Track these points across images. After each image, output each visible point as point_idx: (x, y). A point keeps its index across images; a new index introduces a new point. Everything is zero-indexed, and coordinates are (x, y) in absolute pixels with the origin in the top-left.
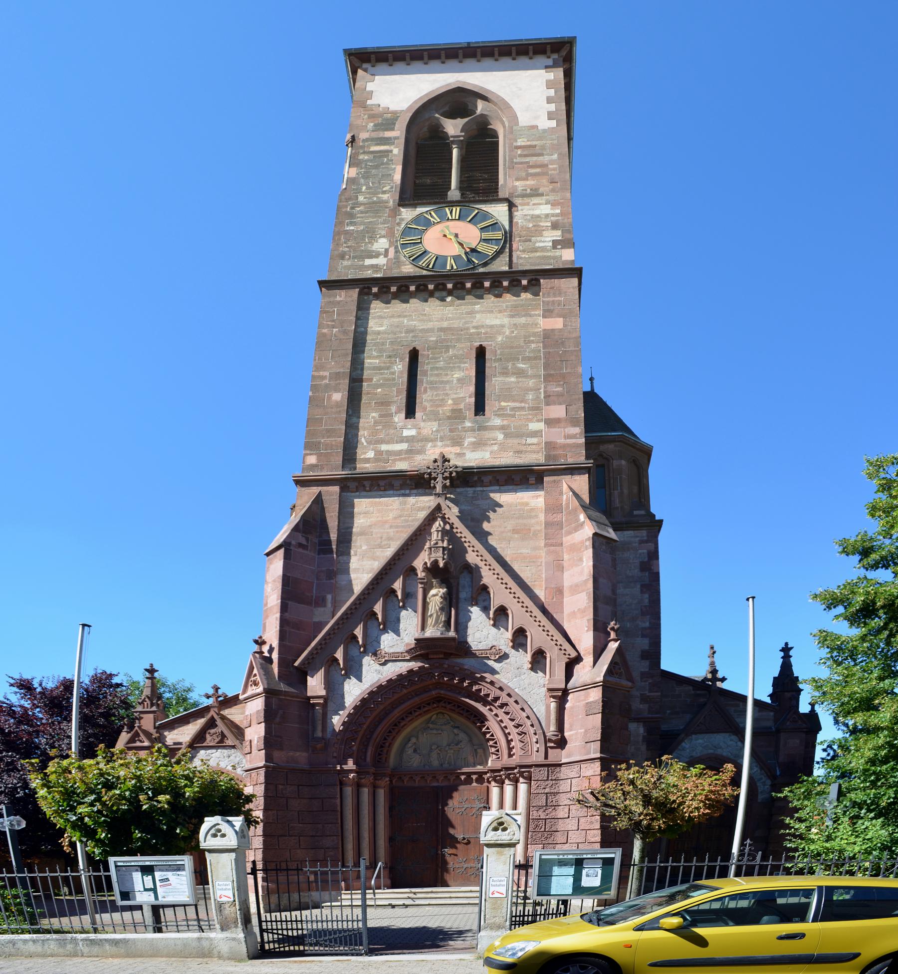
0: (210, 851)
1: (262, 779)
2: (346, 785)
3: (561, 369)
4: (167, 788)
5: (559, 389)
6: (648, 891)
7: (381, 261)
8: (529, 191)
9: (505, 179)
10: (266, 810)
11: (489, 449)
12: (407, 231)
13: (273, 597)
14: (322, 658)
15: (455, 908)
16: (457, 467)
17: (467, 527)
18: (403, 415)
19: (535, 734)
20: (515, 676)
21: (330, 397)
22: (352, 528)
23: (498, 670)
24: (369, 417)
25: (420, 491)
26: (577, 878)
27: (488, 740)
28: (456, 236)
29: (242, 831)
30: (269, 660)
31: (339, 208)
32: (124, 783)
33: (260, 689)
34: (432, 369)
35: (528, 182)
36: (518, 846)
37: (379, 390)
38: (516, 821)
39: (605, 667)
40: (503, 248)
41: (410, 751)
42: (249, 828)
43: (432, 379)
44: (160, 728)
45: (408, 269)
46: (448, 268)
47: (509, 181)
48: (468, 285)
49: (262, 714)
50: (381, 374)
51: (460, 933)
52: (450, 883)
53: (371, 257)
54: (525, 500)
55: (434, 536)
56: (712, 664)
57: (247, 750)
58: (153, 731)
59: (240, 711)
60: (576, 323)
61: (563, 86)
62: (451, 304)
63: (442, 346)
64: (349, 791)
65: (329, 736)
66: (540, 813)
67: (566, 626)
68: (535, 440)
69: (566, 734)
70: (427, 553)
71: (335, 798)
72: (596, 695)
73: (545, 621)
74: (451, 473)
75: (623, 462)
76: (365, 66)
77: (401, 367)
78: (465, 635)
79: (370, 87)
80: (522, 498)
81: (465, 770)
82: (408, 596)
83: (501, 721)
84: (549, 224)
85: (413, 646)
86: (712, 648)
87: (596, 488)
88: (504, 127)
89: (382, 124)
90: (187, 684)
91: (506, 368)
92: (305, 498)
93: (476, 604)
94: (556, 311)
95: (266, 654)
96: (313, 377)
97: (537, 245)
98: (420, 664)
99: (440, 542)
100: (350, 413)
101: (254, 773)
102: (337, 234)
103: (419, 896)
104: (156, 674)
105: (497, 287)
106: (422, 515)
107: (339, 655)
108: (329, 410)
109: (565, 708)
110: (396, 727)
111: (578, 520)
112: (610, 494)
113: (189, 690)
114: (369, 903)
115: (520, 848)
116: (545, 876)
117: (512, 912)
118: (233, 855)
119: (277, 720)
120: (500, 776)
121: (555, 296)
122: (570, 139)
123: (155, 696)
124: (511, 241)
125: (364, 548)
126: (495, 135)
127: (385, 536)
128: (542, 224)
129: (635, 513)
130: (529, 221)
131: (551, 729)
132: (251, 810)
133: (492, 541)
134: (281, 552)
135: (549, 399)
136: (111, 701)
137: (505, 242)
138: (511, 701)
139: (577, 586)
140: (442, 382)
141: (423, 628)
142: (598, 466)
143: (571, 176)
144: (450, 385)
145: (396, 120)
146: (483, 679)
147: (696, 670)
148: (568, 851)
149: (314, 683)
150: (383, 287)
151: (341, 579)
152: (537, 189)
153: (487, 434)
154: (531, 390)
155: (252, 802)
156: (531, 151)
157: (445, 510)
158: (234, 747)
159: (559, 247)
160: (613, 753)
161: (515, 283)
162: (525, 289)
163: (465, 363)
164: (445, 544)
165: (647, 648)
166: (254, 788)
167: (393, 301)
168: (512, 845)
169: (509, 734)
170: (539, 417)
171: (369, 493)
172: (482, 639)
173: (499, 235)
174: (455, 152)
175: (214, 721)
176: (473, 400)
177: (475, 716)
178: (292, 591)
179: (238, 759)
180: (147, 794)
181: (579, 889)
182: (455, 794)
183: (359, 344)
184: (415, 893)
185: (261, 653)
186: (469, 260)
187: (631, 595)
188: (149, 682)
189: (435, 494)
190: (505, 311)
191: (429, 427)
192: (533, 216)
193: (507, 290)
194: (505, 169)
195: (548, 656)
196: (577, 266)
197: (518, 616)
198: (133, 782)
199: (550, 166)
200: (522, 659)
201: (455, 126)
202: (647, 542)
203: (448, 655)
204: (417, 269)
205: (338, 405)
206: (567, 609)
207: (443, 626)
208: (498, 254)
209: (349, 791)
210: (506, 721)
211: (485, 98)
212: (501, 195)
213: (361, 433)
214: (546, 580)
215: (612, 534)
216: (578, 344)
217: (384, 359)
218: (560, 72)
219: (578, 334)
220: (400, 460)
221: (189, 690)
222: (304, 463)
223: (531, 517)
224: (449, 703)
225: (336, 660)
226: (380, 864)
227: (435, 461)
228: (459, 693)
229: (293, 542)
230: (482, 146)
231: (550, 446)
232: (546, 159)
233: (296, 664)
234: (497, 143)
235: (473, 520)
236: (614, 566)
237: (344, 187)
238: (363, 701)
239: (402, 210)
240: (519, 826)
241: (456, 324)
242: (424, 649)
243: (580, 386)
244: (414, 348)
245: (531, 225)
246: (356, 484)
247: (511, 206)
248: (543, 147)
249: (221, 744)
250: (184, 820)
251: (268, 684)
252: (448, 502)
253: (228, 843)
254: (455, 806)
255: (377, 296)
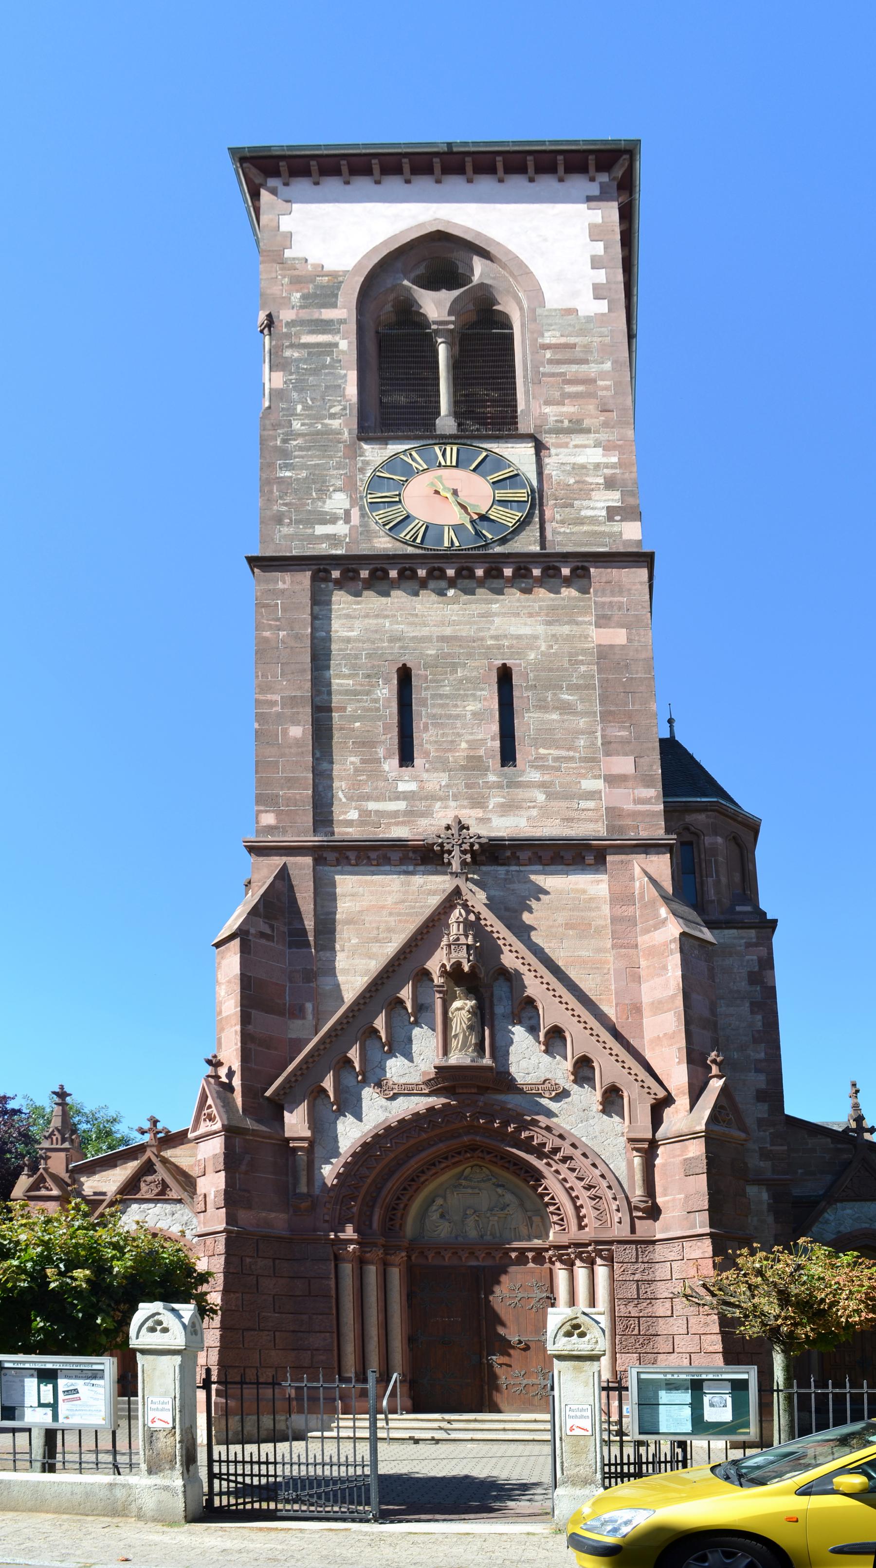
0: (144, 1352)
1: (221, 1247)
2: (344, 1260)
3: (626, 704)
4: (87, 1260)
5: (624, 733)
6: (804, 1431)
7: (340, 529)
8: (566, 423)
9: (527, 402)
10: (226, 1292)
11: (525, 813)
12: (376, 482)
13: (229, 1003)
14: (304, 1087)
15: (513, 1446)
16: (479, 837)
17: (499, 917)
18: (396, 761)
19: (615, 1199)
20: (578, 1117)
21: (285, 732)
22: (335, 913)
23: (556, 1112)
24: (345, 764)
25: (429, 867)
26: (697, 1407)
27: (547, 1205)
28: (455, 493)
29: (193, 1324)
30: (229, 1088)
31: (263, 441)
32: (25, 1250)
33: (218, 1126)
34: (434, 696)
35: (565, 409)
36: (602, 1358)
37: (357, 724)
38: (598, 1323)
39: (707, 1113)
40: (530, 515)
41: (435, 1216)
42: (203, 1319)
43: (434, 711)
44: (76, 1172)
45: (383, 544)
46: (446, 544)
47: (534, 405)
48: (480, 572)
49: (222, 1159)
50: (359, 701)
51: (524, 1488)
52: (502, 1406)
53: (324, 522)
54: (581, 886)
55: (454, 929)
56: (856, 1107)
57: (201, 1207)
58: (65, 1176)
59: (188, 1153)
60: (647, 637)
61: (618, 237)
62: (455, 601)
63: (446, 663)
64: (347, 1269)
65: (317, 1191)
66: (630, 1307)
67: (648, 1056)
68: (591, 804)
69: (660, 1200)
70: (445, 951)
71: (328, 1278)
72: (697, 1149)
73: (617, 1048)
74: (472, 845)
75: (719, 840)
76: (272, 182)
77: (386, 692)
78: (507, 1064)
79: (286, 224)
80: (576, 884)
81: (516, 1245)
82: (422, 1009)
83: (565, 1180)
84: (601, 480)
85: (432, 1076)
86: (854, 1085)
87: (680, 873)
88: (521, 309)
89: (315, 296)
90: (112, 1113)
91: (545, 700)
92: (264, 872)
93: (520, 1023)
94: (615, 618)
95: (224, 1079)
96: (257, 701)
97: (584, 513)
98: (444, 1100)
99: (462, 938)
100: (318, 755)
101: (210, 1240)
102: (266, 483)
103: (456, 1425)
104: (68, 1099)
105: (524, 576)
106: (434, 901)
107: (328, 1084)
108: (287, 751)
109: (654, 1166)
110: (414, 1183)
111: (657, 915)
112: (702, 883)
113: (114, 1121)
114: (381, 1434)
115: (605, 1361)
116: (648, 1406)
117: (603, 1458)
118: (178, 1359)
119: (243, 1168)
120: (568, 1254)
121: (613, 595)
122: (631, 336)
123: (68, 1128)
124: (541, 505)
125: (354, 941)
126: (505, 322)
127: (383, 926)
128: (590, 479)
129: (738, 908)
130: (569, 474)
131: (637, 1193)
132: (206, 1294)
133: (535, 937)
134: (236, 943)
135: (609, 747)
136: (6, 1132)
137: (533, 506)
138: (577, 1153)
139: (660, 1002)
140: (450, 717)
141: (446, 1052)
142: (683, 844)
143: (634, 401)
144: (461, 720)
145: (339, 288)
146: (535, 1123)
147: (833, 1114)
148: (673, 1364)
149: (294, 1121)
150: (349, 570)
151: (325, 983)
152: (579, 422)
153: (521, 794)
154: (583, 733)
155: (208, 1282)
156: (566, 353)
157: (466, 895)
158: (180, 1201)
159: (618, 518)
160: (729, 1232)
161: (551, 572)
162: (568, 582)
163: (483, 689)
164: (470, 941)
165: (763, 1086)
166: (209, 1260)
167: (366, 593)
168: (595, 1358)
169: (577, 1197)
170: (597, 773)
171: (356, 868)
172: (530, 1070)
173: (522, 494)
174: (442, 351)
175: (153, 1166)
176: (497, 744)
177: (527, 1172)
178: (255, 996)
179: (185, 1218)
180: (57, 1266)
181: (700, 1425)
182: (504, 1278)
183: (320, 656)
184: (449, 1422)
185: (217, 1077)
186: (478, 534)
187: (738, 1017)
188: (58, 1110)
189: (451, 873)
190: (538, 614)
191: (436, 781)
192: (574, 466)
193: (540, 582)
194: (525, 383)
195: (625, 1094)
196: (646, 549)
197: (581, 1038)
198: (39, 1249)
199: (600, 383)
200: (588, 1098)
201: (438, 304)
202: (756, 945)
203: (483, 1090)
204: (398, 544)
205: (297, 742)
206: (648, 1034)
207: (474, 1051)
208: (523, 524)
209: (347, 1269)
210: (572, 1181)
211: (485, 254)
212: (524, 427)
213: (336, 784)
214: (616, 993)
215: (707, 934)
216: (649, 668)
217: (360, 679)
218: (611, 212)
219: (649, 654)
220: (397, 824)
221: (114, 1121)
222: (257, 822)
223: (590, 909)
224: (489, 1153)
225: (324, 1091)
226: (395, 1375)
227: (448, 828)
228: (503, 1141)
229: (252, 931)
230: (486, 339)
231: (612, 812)
232: (592, 369)
233: (268, 1094)
234: (510, 338)
235: (507, 909)
236: (712, 977)
237: (267, 404)
238: (365, 1145)
239: (365, 446)
240: (603, 1331)
241: (465, 631)
242: (446, 1079)
243: (655, 730)
244: (404, 665)
245: (572, 481)
246: (336, 855)
247: (540, 447)
248: (587, 348)
249: (162, 1196)
250: (109, 1305)
251: (228, 1119)
252: (470, 885)
253: (172, 1342)
254: (507, 1294)
255: (339, 584)
